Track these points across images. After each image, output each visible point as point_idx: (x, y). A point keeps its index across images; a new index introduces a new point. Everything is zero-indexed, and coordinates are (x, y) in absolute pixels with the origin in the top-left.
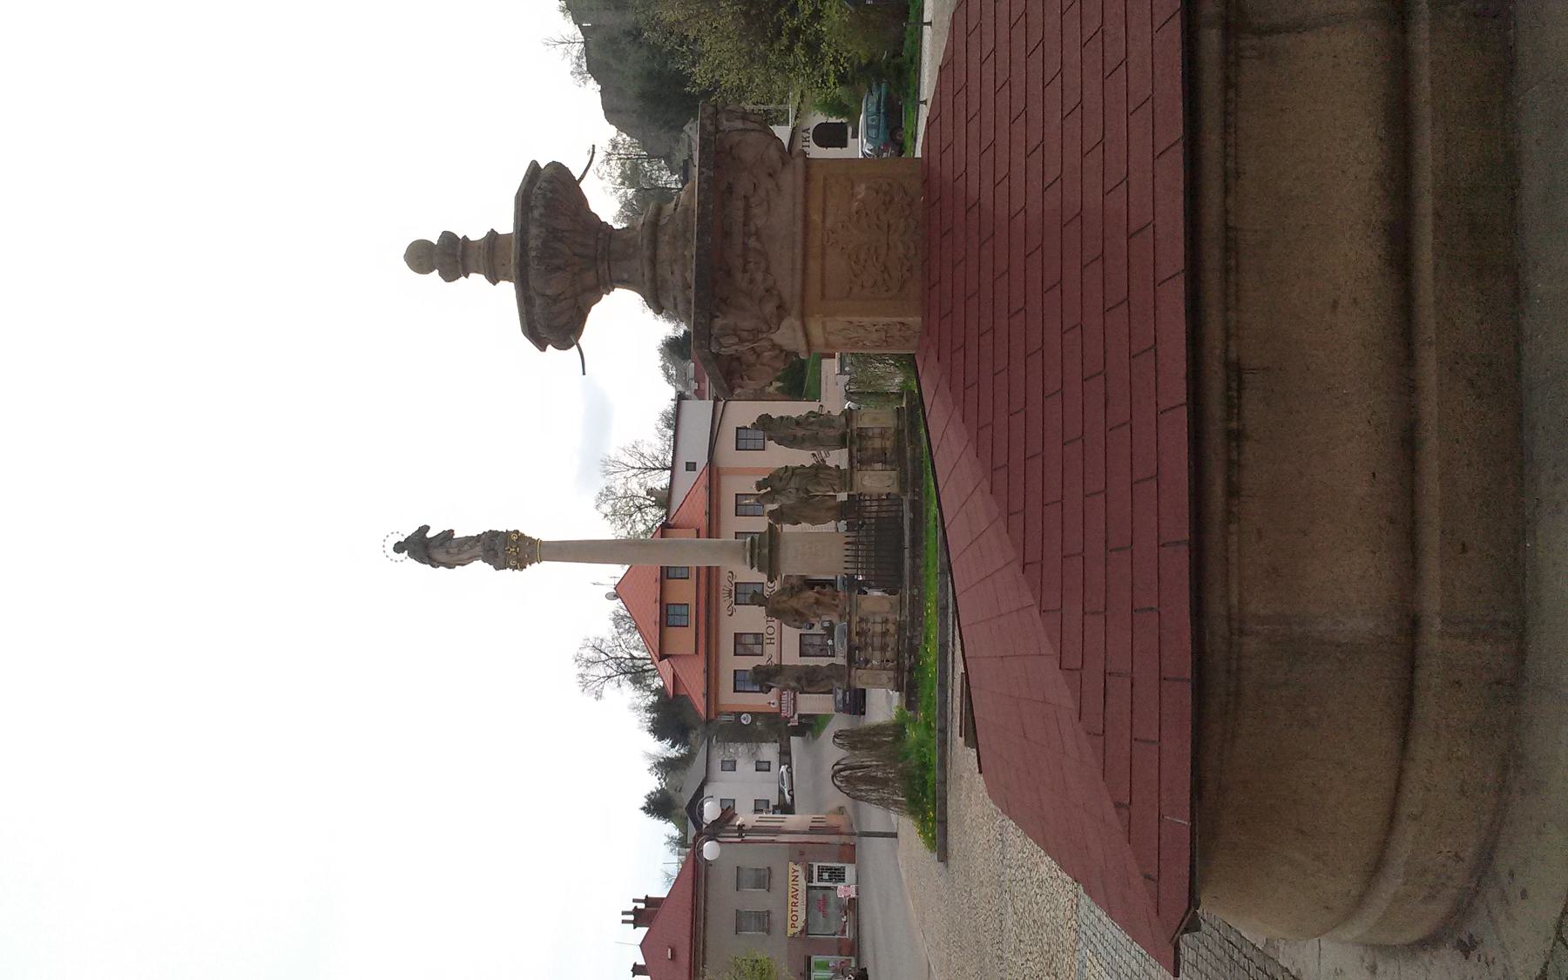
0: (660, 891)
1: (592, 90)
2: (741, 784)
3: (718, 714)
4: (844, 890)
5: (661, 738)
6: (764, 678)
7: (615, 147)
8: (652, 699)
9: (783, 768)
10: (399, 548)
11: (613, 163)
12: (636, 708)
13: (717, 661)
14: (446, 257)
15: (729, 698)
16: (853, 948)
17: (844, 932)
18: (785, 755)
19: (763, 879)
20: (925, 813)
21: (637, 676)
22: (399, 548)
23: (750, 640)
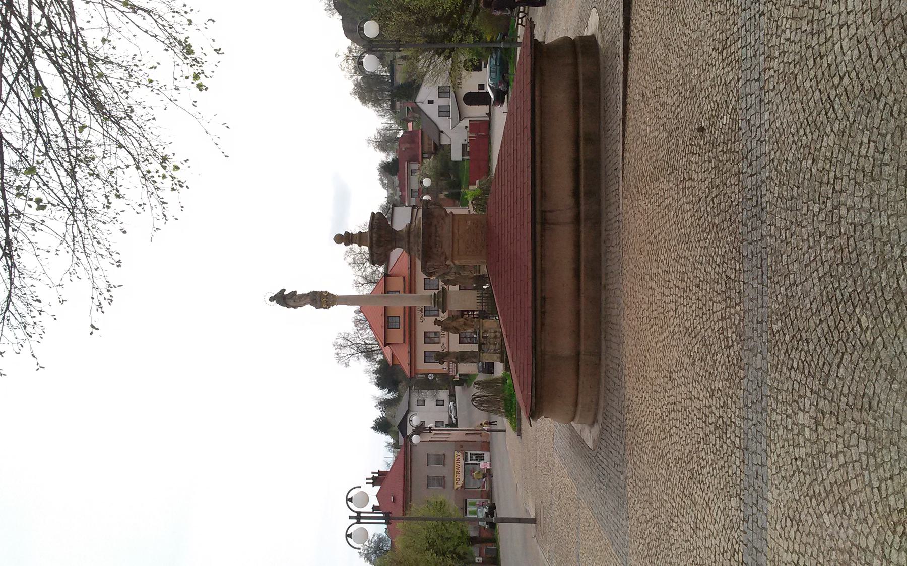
0: (384, 468)
1: (337, 18)
2: (427, 411)
3: (416, 374)
4: (484, 465)
5: (382, 388)
6: (441, 357)
7: (350, 51)
8: (377, 366)
9: (451, 404)
10: (271, 299)
11: (350, 62)
12: (368, 372)
13: (415, 345)
14: (346, 239)
15: (422, 366)
16: (489, 494)
17: (484, 486)
18: (452, 397)
19: (441, 460)
20: (512, 415)
21: (368, 354)
22: (271, 299)
23: (432, 335)
